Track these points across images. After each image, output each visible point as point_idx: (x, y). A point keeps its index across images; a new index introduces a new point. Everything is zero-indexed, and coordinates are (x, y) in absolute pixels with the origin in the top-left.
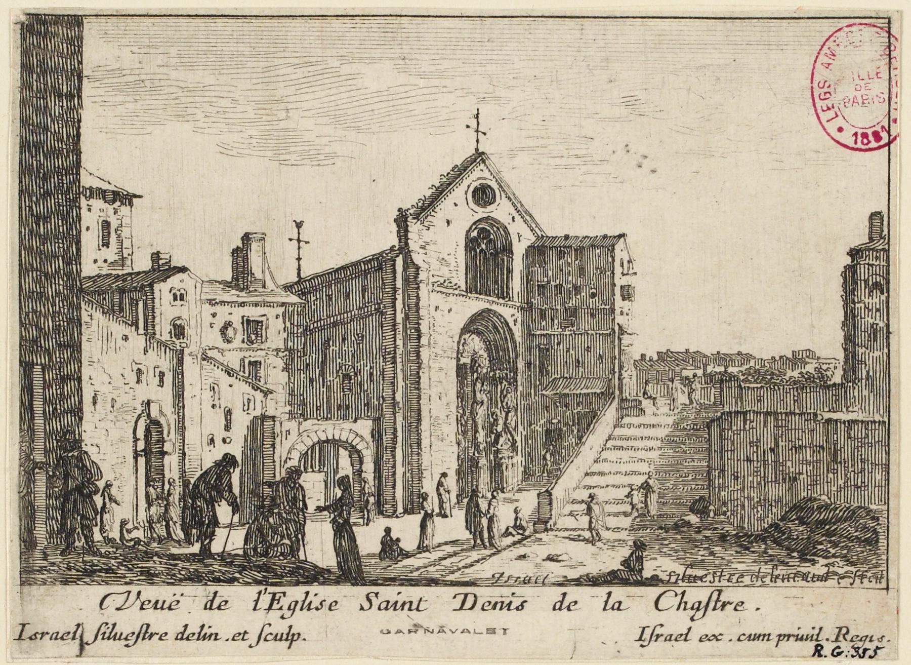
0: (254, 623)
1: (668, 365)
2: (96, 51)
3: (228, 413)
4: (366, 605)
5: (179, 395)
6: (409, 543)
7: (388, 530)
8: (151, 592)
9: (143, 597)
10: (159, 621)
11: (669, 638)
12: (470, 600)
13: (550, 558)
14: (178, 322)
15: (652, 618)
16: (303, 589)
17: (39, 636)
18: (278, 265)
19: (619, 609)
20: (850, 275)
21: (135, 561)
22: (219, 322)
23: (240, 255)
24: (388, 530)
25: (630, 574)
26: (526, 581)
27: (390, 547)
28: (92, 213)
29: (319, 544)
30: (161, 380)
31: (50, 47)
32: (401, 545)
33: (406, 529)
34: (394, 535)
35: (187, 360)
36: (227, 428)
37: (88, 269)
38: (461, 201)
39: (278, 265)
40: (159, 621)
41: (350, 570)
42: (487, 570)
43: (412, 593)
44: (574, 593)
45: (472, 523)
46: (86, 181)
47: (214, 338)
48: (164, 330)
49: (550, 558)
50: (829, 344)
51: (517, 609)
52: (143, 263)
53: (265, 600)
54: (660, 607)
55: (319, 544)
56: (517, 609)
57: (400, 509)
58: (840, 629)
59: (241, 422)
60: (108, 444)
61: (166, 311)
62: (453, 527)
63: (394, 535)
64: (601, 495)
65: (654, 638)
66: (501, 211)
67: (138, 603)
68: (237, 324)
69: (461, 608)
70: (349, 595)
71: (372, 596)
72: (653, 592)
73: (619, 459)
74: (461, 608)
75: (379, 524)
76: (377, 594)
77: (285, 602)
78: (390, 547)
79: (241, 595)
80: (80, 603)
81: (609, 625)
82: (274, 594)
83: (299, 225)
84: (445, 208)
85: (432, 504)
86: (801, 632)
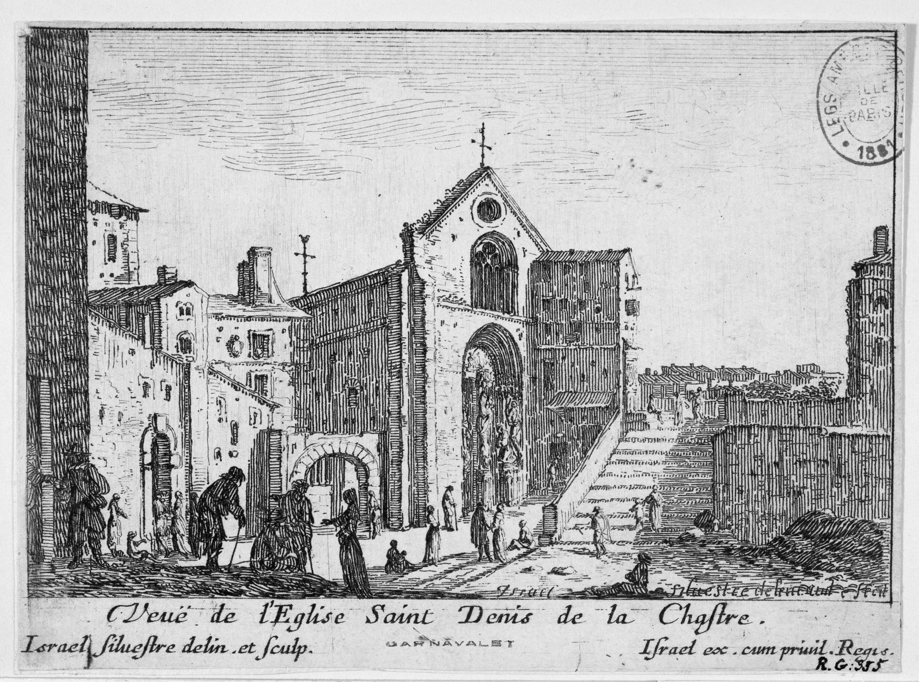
0: (261, 635)
1: (672, 380)
2: (102, 65)
3: (235, 426)
4: (372, 618)
6: (415, 556)
7: (394, 544)
8: (159, 605)
9: (151, 610)
10: (167, 633)
11: (674, 651)
13: (555, 571)
14: (185, 336)
15: (657, 632)
16: (309, 602)
17: (47, 648)
18: (284, 279)
19: (623, 622)
20: (855, 289)
22: (225, 337)
23: (246, 269)
24: (394, 544)
25: (634, 587)
26: (531, 594)
27: (396, 560)
28: (98, 228)
29: (325, 558)
30: (168, 394)
31: (56, 60)
33: (412, 543)
34: (400, 548)
35: (194, 374)
36: (234, 441)
37: (95, 283)
39: (284, 279)
40: (167, 633)
44: (579, 605)
45: (477, 536)
46: (92, 195)
47: (220, 352)
48: (170, 344)
49: (555, 571)
50: (833, 359)
51: (522, 621)
52: (149, 277)
53: (272, 612)
54: (665, 620)
56: (522, 621)
57: (406, 523)
58: (844, 642)
59: (248, 436)
60: (115, 457)
62: (460, 540)
63: (400, 548)
64: (606, 508)
65: (658, 651)
66: (506, 226)
67: (146, 616)
68: (243, 338)
69: (467, 621)
70: (355, 608)
71: (378, 609)
72: (659, 605)
73: (625, 472)
74: (467, 621)
75: (385, 537)
76: (383, 607)
77: (292, 615)
78: (396, 560)
79: (247, 608)
80: (88, 615)
81: (613, 639)
82: (281, 607)
83: (305, 240)
84: (450, 223)
86: (805, 646)
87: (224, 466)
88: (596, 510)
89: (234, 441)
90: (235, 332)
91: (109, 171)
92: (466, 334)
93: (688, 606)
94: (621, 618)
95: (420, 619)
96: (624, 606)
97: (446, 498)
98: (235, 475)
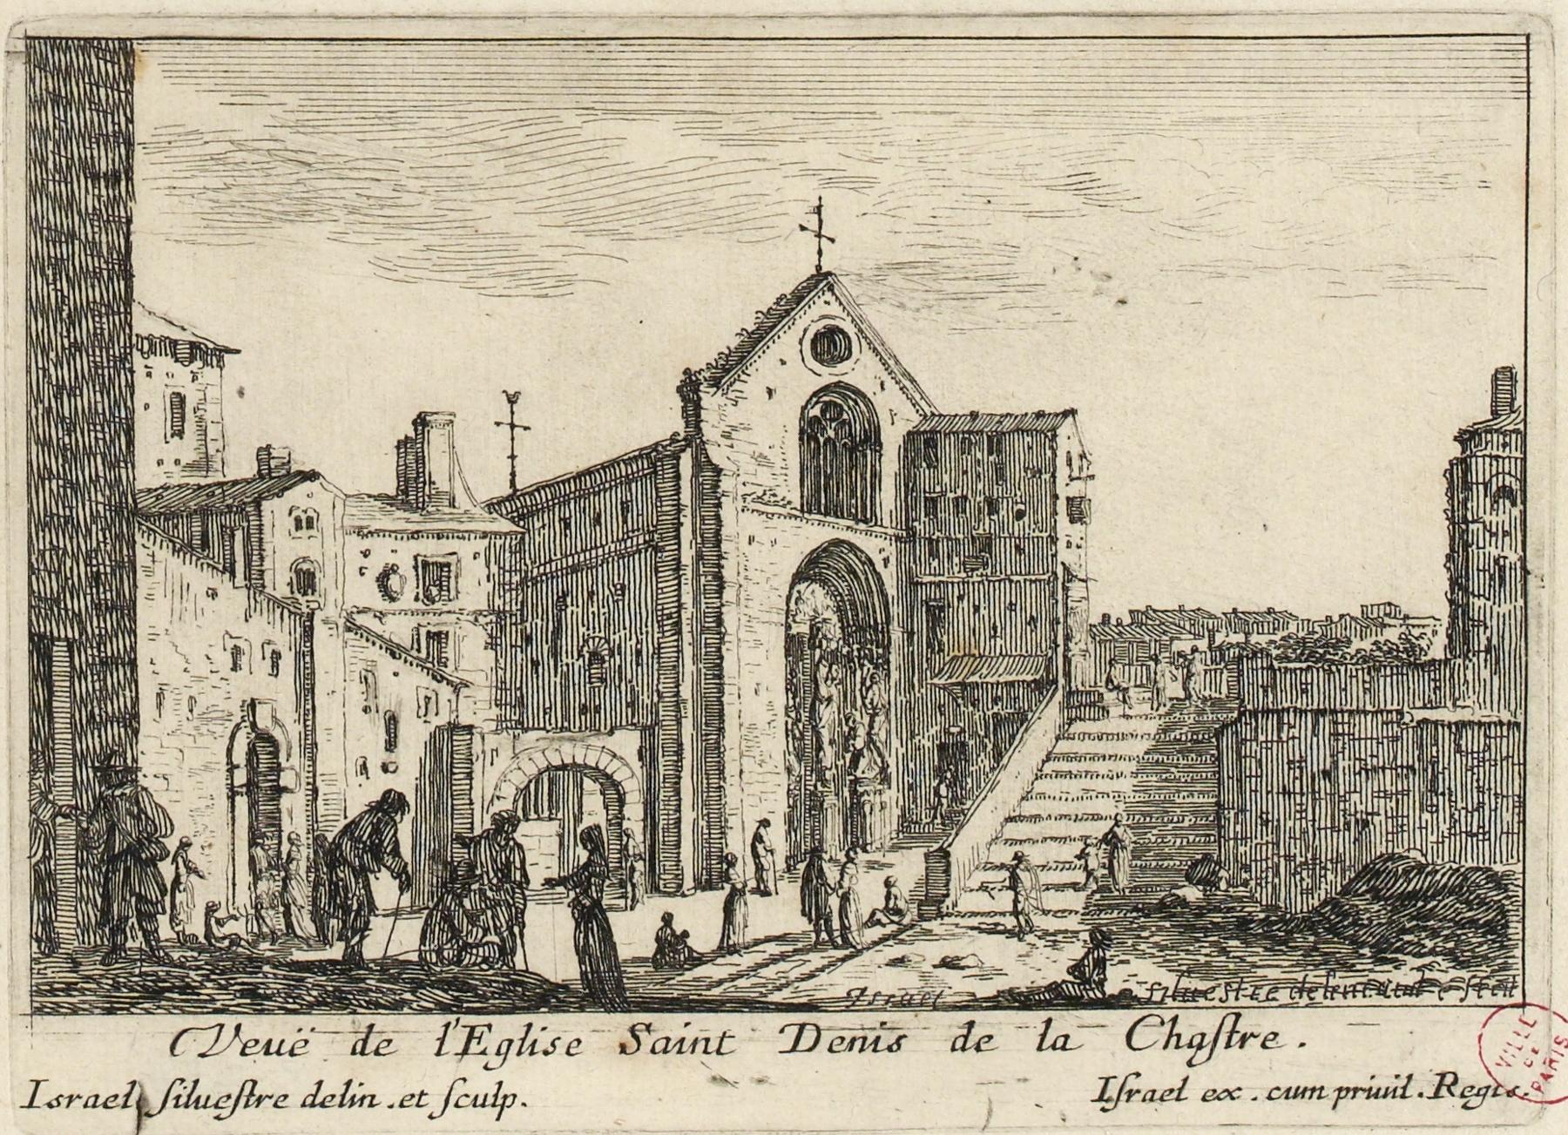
0: (437, 1076)
1: (1144, 635)
2: (156, 99)
3: (392, 722)
5: (306, 688)
6: (704, 937)
7: (667, 919)
8: (258, 1027)
11: (1151, 1097)
12: (809, 1037)
15: (1121, 1063)
16: (523, 1019)
17: (64, 1102)
18: (476, 468)
19: (1063, 1048)
20: (1459, 477)
21: (233, 976)
22: (375, 566)
23: (412, 448)
24: (667, 919)
25: (1081, 991)
26: (905, 1003)
27: (671, 947)
28: (156, 380)
29: (548, 942)
30: (275, 665)
32: (690, 942)
33: (699, 918)
35: (320, 631)
36: (391, 745)
38: (792, 354)
39: (476, 468)
40: (272, 1074)
41: (602, 987)
42: (839, 982)
43: (708, 1024)
44: (987, 1021)
46: (143, 325)
48: (279, 581)
50: (1427, 596)
52: (242, 466)
53: (456, 1040)
54: (1135, 1044)
55: (548, 942)
56: (890, 1049)
57: (689, 883)
58: (1443, 1076)
59: (414, 736)
60: (183, 775)
61: (283, 550)
62: (777, 913)
66: (861, 371)
68: (406, 567)
72: (1121, 1019)
76: (648, 1027)
78: (671, 947)
79: (415, 1032)
82: (473, 1029)
83: (512, 400)
85: (744, 872)
87: (373, 790)
88: (1018, 858)
89: (391, 745)
90: (392, 559)
91: (172, 282)
92: (791, 561)
93: (1175, 1020)
94: (1060, 1043)
95: (713, 1046)
96: (1065, 1021)
97: (757, 838)
98: (390, 804)
